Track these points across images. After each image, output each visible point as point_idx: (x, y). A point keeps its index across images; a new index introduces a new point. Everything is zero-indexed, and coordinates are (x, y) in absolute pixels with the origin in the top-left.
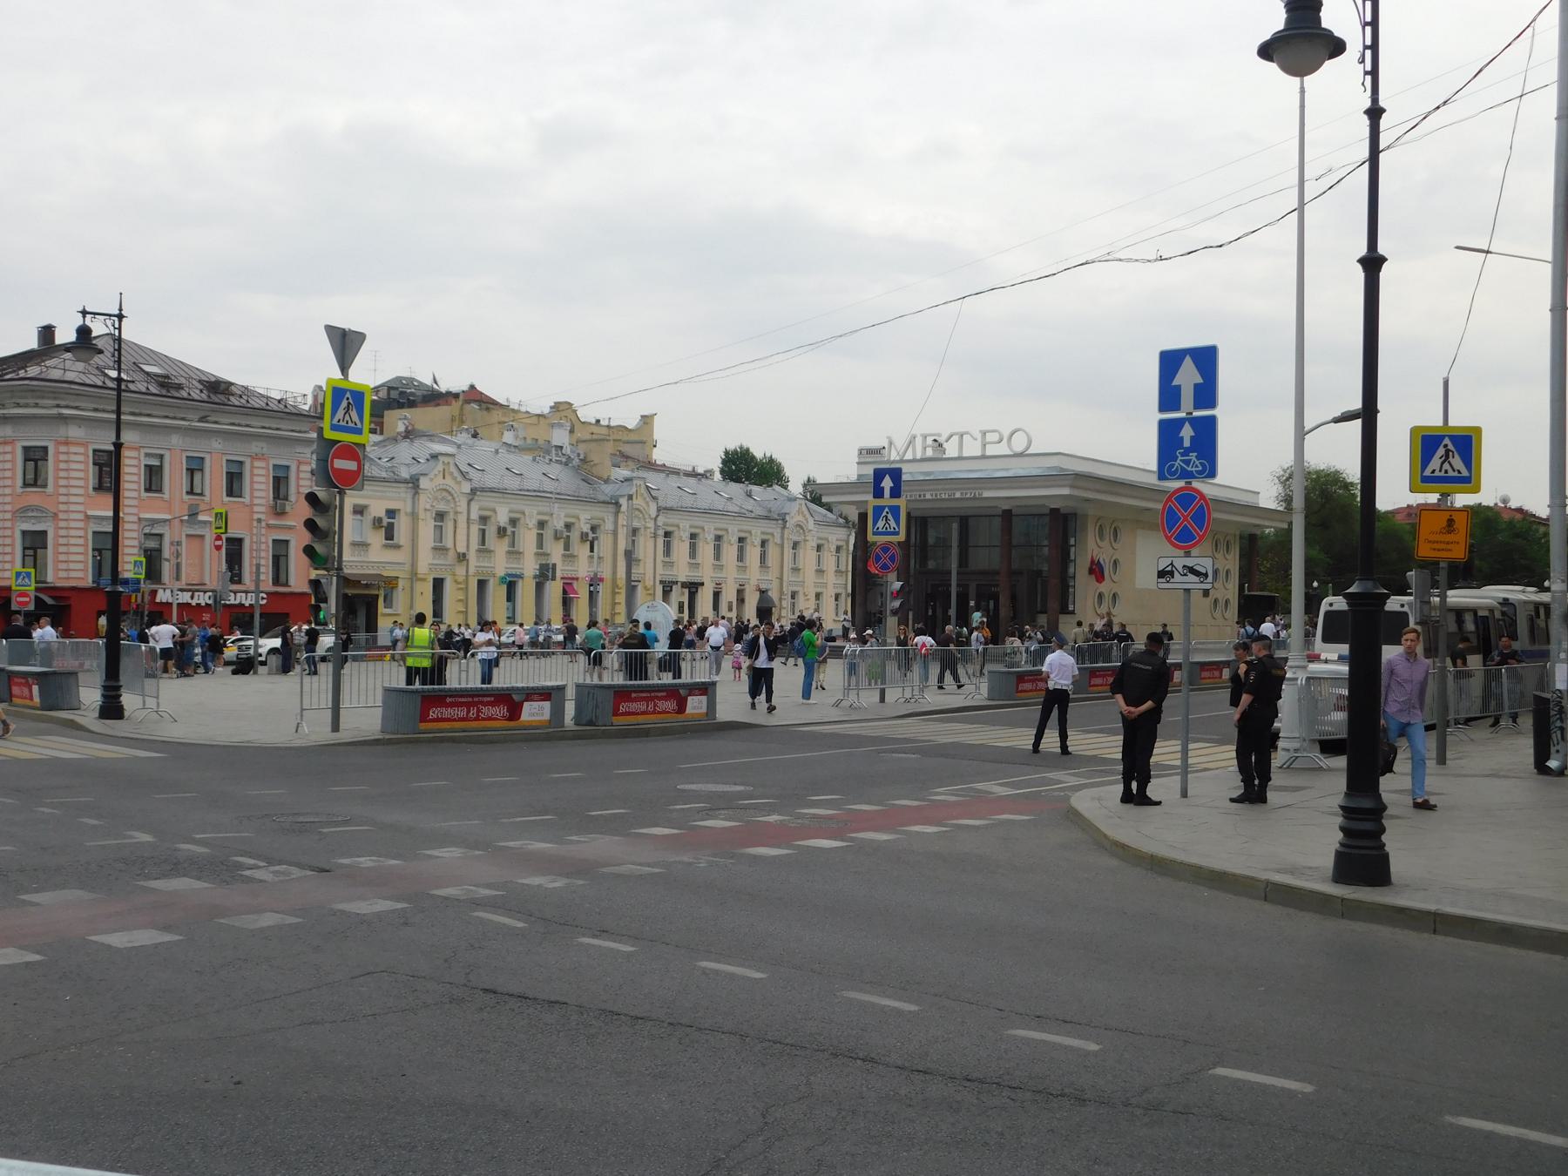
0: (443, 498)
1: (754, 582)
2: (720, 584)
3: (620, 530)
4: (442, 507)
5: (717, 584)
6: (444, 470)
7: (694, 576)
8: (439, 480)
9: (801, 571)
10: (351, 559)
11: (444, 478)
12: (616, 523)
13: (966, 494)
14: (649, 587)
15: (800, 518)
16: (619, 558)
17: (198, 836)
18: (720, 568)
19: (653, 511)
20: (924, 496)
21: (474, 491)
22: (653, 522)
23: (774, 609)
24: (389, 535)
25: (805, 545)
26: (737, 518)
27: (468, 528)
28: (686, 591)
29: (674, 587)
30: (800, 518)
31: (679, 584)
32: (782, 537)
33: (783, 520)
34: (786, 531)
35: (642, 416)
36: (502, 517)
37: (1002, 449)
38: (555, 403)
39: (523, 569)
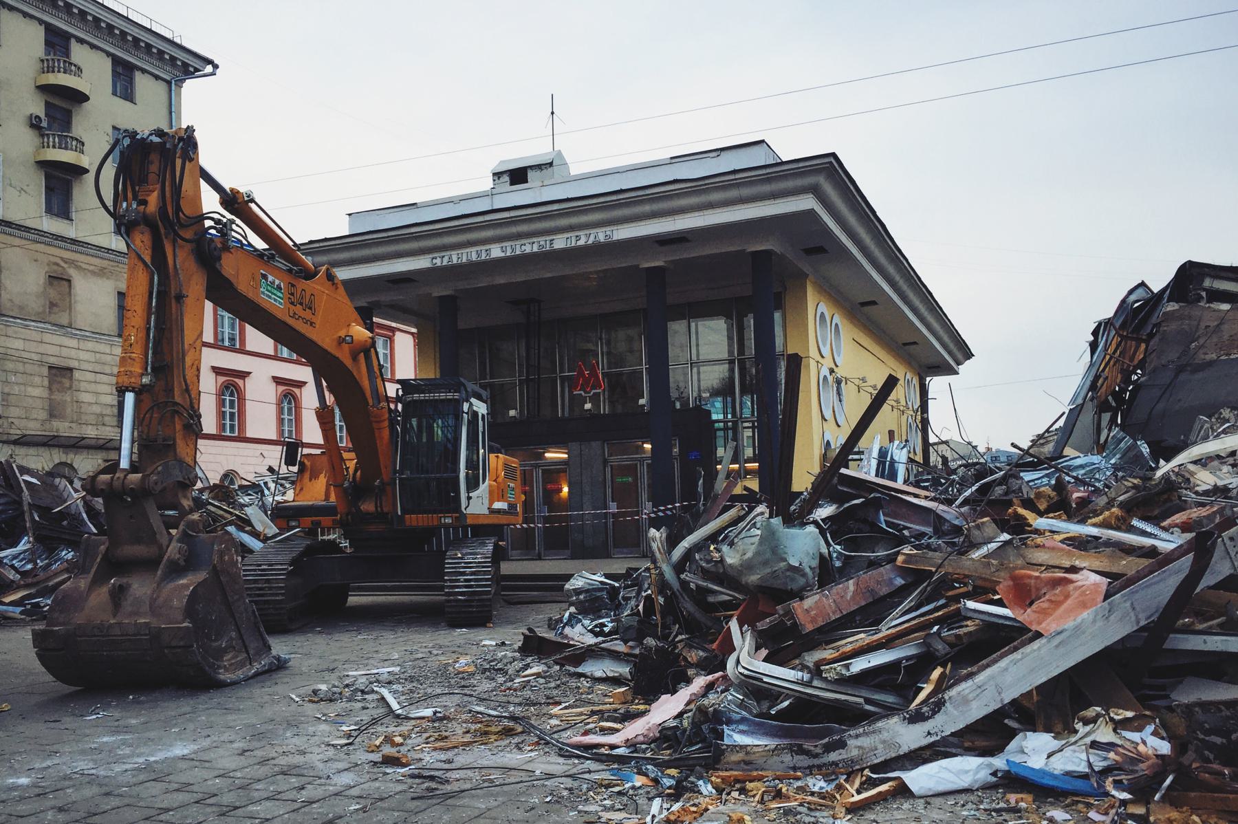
13: (578, 237)
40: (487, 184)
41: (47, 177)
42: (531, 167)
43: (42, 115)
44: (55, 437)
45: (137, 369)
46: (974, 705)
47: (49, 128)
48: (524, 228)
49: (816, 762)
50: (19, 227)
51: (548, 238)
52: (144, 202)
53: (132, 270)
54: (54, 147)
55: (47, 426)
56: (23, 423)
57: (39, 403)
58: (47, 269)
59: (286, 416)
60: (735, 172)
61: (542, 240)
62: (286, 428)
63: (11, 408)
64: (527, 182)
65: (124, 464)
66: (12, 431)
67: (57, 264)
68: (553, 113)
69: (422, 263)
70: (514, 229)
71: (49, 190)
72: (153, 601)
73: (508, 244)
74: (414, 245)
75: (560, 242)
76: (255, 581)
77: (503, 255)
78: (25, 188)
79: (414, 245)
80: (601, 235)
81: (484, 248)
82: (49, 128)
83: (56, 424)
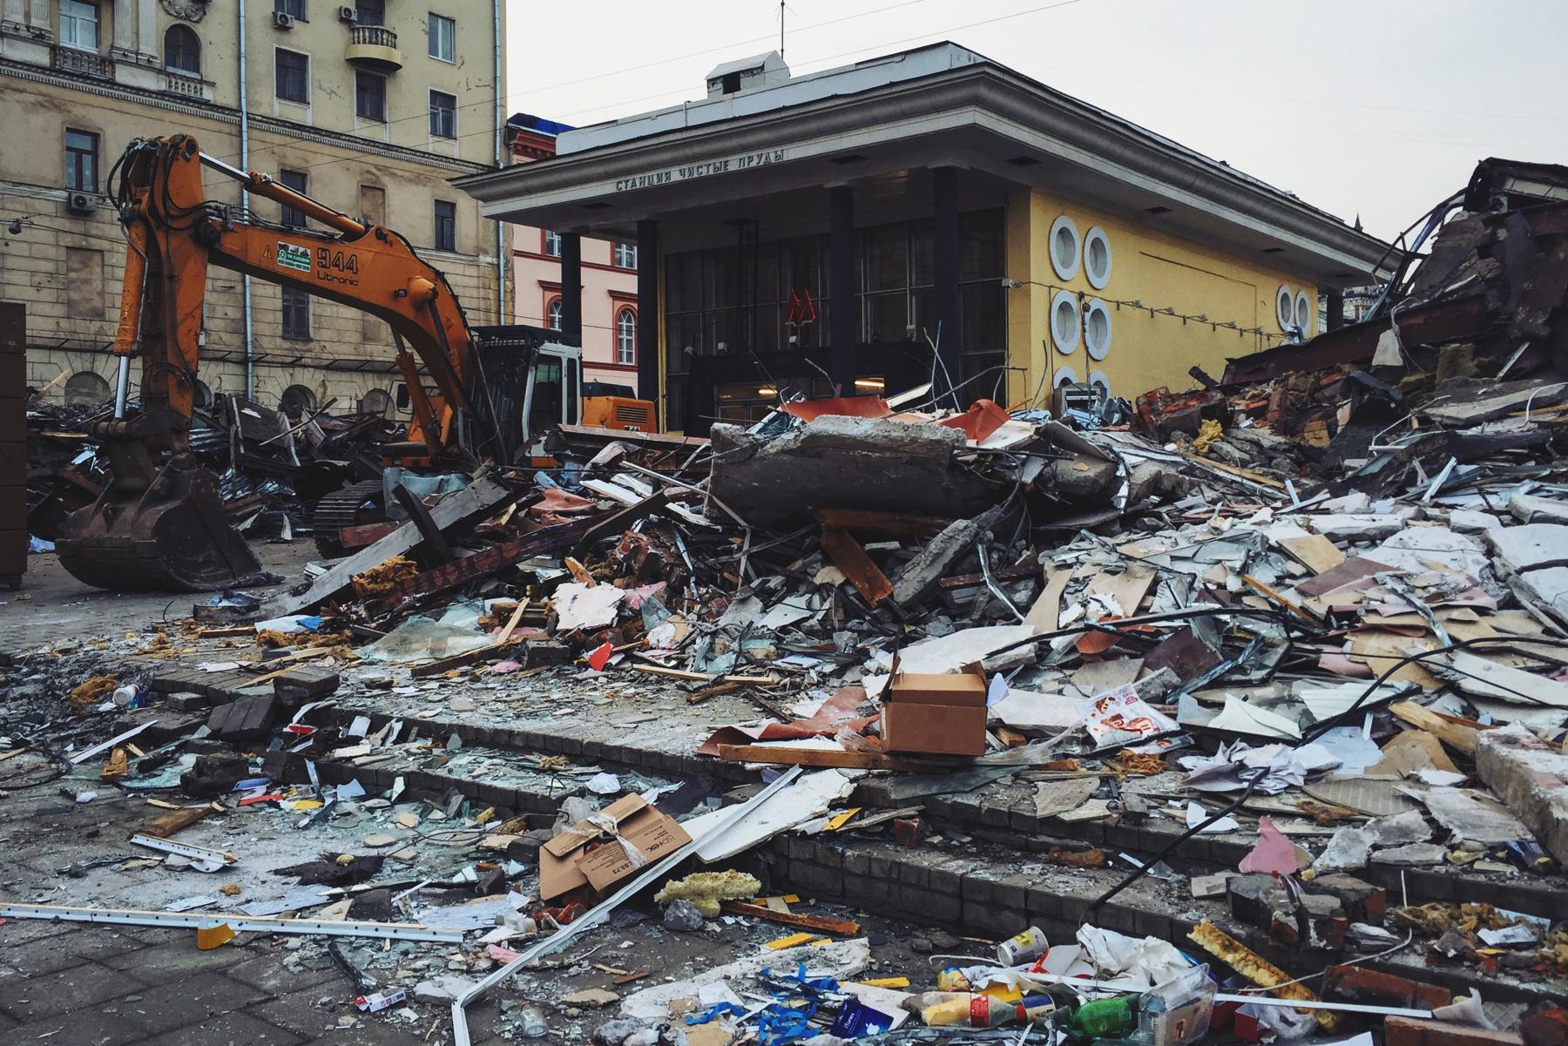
13: (751, 159)
40: (701, 93)
41: (359, 76)
42: (743, 72)
43: (352, 7)
44: (367, 361)
45: (129, 339)
46: (327, 586)
47: (360, 21)
48: (697, 150)
49: (244, 617)
50: (330, 134)
51: (723, 160)
52: (139, 201)
53: (129, 256)
54: (364, 42)
55: (361, 350)
56: (336, 347)
57: (350, 325)
58: (359, 178)
59: (624, 336)
60: (892, 84)
61: (717, 161)
62: (625, 350)
63: (323, 331)
64: (739, 89)
65: (118, 414)
66: (324, 356)
67: (368, 172)
68: (783, 4)
69: (607, 188)
70: (689, 151)
71: (361, 90)
72: (134, 522)
73: (686, 167)
74: (600, 170)
75: (734, 165)
76: (330, 514)
77: (681, 178)
78: (335, 89)
79: (600, 170)
80: (772, 155)
81: (663, 171)
82: (360, 21)
83: (369, 348)
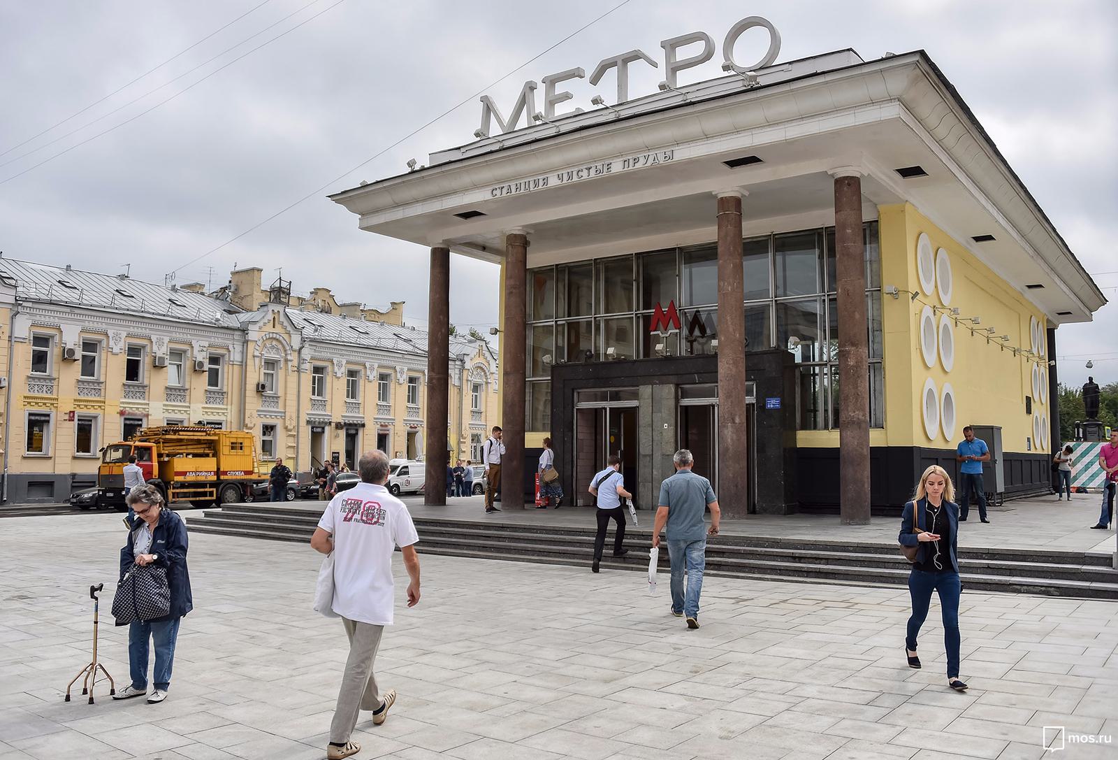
0: (273, 347)
1: (66, 405)
2: (386, 426)
3: (250, 362)
4: (273, 355)
5: (411, 427)
6: (274, 318)
7: (353, 416)
8: (269, 328)
9: (483, 414)
10: (262, 409)
11: (274, 327)
12: (244, 353)
13: (636, 160)
14: (289, 427)
15: (481, 360)
16: (248, 393)
17: (151, 641)
18: (388, 409)
19: (296, 341)
20: (546, 181)
21: (18, 302)
22: (296, 354)
23: (451, 452)
24: (214, 379)
25: (487, 387)
26: (406, 356)
27: (11, 348)
28: (342, 433)
29: (327, 428)
30: (478, 360)
31: (333, 425)
32: (460, 379)
33: (461, 361)
34: (465, 373)
35: (393, 304)
36: (71, 336)
37: (712, 70)
38: (314, 289)
39: (331, 416)
